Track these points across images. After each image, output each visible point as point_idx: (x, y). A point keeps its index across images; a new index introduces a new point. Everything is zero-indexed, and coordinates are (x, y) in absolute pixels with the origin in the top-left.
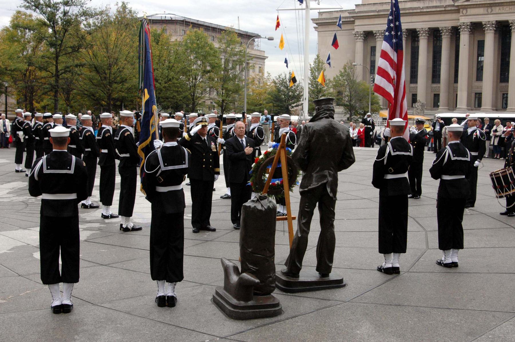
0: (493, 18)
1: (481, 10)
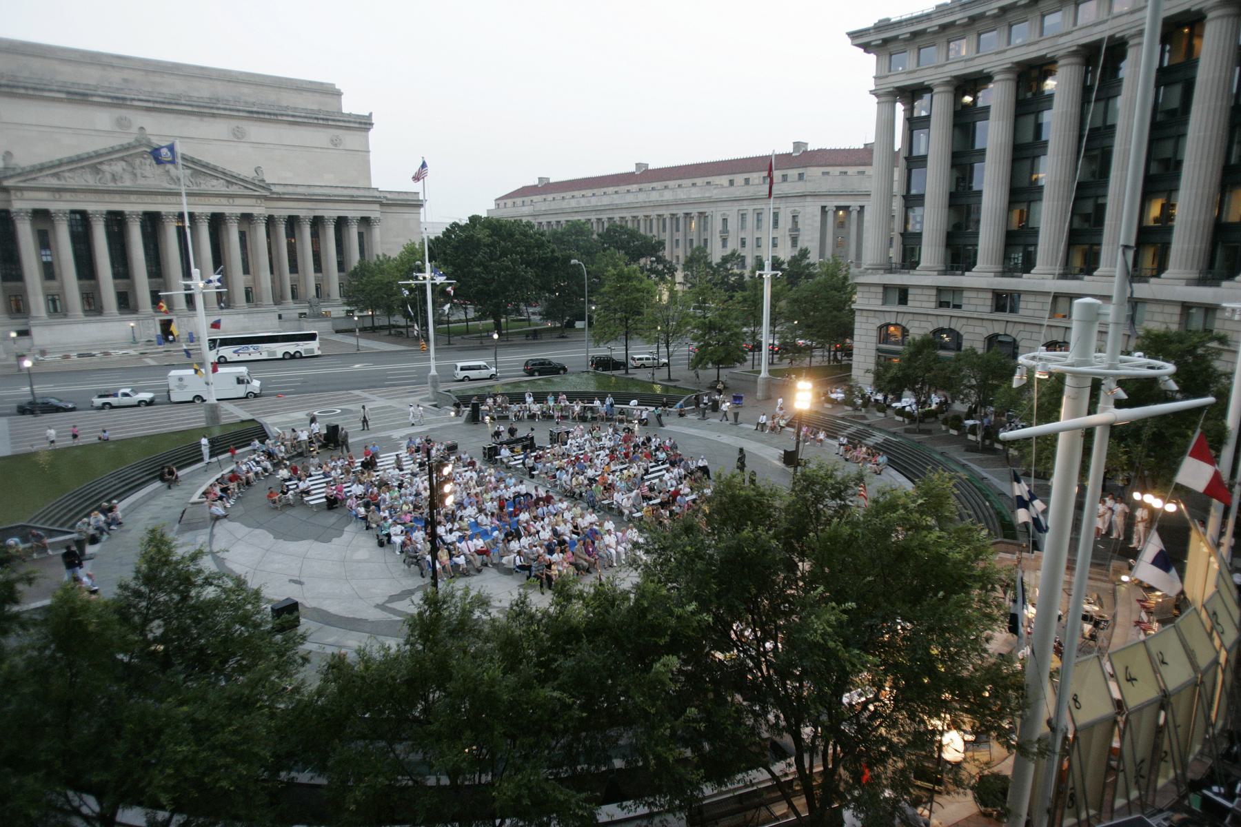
0: (141, 208)
1: (44, 195)
